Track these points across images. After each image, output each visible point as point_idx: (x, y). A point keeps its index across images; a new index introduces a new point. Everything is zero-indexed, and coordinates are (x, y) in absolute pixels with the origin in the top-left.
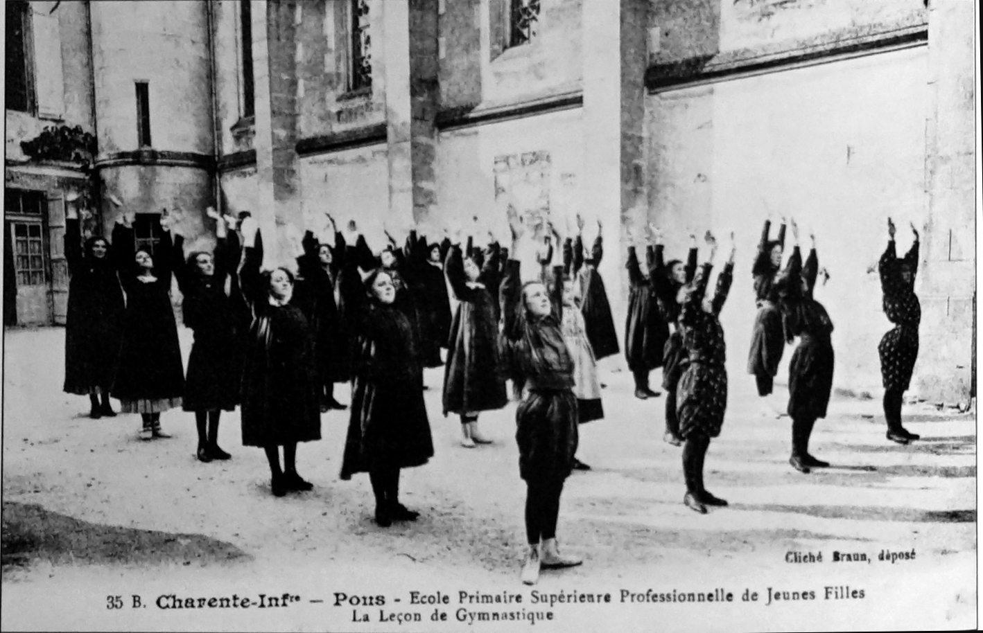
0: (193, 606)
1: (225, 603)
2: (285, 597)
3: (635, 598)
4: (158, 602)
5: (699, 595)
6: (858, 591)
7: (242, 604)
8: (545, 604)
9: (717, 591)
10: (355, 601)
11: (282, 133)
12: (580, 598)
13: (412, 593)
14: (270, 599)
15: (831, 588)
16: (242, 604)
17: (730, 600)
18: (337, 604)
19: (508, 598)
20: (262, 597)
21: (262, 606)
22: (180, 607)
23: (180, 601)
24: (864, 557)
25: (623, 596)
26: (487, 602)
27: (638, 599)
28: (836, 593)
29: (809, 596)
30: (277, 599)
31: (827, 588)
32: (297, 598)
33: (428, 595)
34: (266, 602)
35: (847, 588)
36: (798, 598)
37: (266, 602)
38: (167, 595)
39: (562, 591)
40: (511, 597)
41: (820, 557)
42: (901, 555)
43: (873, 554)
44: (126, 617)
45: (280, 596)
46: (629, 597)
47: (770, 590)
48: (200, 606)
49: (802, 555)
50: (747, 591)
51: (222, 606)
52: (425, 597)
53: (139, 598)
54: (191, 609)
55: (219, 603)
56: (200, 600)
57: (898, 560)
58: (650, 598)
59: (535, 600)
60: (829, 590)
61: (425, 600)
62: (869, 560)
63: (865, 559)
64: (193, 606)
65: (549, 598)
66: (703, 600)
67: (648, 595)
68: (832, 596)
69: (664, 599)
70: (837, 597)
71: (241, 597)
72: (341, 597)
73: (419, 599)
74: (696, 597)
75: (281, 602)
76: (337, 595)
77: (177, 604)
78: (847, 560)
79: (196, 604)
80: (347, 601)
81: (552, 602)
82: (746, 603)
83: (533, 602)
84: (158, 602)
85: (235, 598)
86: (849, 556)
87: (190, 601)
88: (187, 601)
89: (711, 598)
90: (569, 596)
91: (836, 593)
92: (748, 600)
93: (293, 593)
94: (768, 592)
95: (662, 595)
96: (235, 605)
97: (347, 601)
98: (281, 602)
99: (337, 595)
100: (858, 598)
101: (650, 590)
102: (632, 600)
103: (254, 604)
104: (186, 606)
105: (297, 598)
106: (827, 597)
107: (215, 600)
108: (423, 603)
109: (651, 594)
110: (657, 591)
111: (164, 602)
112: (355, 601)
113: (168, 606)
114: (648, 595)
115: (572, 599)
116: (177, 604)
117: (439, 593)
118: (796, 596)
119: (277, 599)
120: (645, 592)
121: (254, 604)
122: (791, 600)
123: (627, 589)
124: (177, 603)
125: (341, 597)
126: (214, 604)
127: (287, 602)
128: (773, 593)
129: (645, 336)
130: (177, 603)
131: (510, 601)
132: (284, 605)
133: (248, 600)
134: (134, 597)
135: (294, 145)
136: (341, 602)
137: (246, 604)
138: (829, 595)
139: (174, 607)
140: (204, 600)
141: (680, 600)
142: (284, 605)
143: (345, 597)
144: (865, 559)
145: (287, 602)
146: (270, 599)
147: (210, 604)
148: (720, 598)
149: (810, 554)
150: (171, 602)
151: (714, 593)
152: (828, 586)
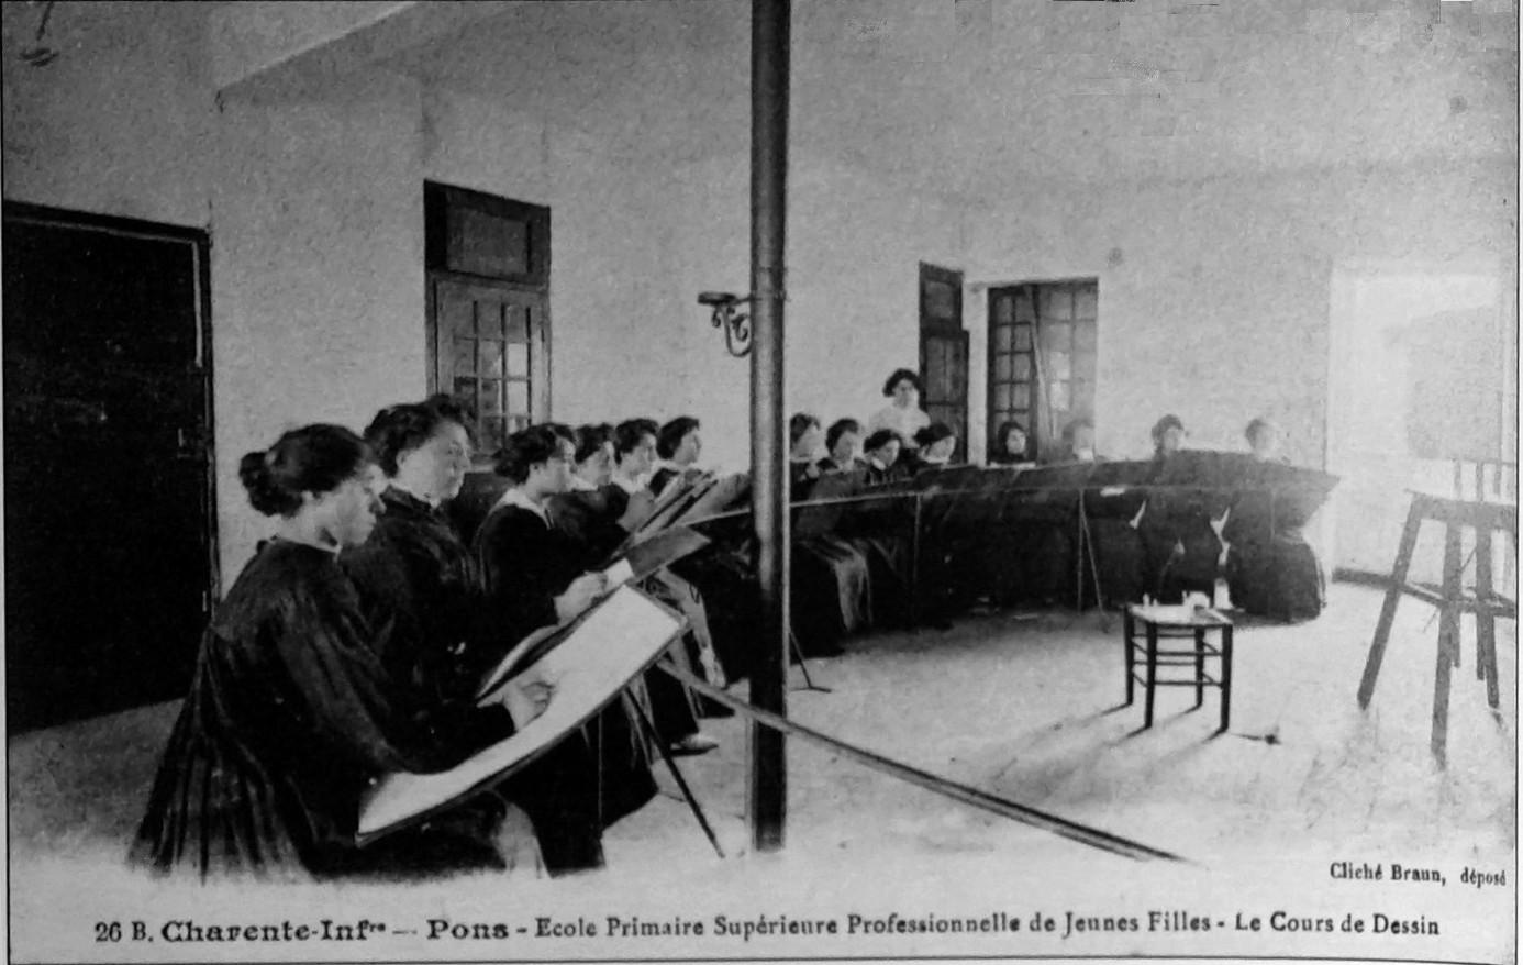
0: (220, 938)
1: (270, 934)
2: (363, 925)
3: (871, 928)
4: (165, 932)
5: (969, 922)
6: (1128, 920)
7: (298, 934)
8: (736, 936)
9: (995, 916)
10: (460, 932)
11: (777, 296)
12: (1356, 926)
13: (540, 920)
14: (340, 929)
15: (1159, 914)
16: (298, 934)
17: (1360, 931)
18: (433, 935)
19: (682, 928)
20: (327, 924)
21: (327, 936)
22: (200, 938)
23: (199, 930)
24: (1436, 875)
25: (851, 925)
26: (650, 933)
27: (876, 929)
28: (1167, 922)
29: (1129, 925)
30: (275, 930)
31: (540, 920)
32: (382, 927)
33: (564, 924)
34: (333, 932)
35: (1184, 914)
36: (1113, 928)
37: (333, 932)
38: (179, 921)
39: (762, 917)
40: (687, 926)
41: (1379, 872)
42: (1489, 879)
43: (1452, 872)
44: (126, 948)
45: (354, 925)
46: (862, 926)
47: (1069, 915)
48: (231, 938)
49: (1355, 868)
50: (1038, 915)
51: (266, 938)
52: (559, 926)
53: (144, 926)
54: (216, 942)
55: (261, 934)
56: (231, 930)
57: (1485, 885)
58: (894, 926)
59: (720, 929)
60: (1156, 917)
61: (558, 930)
62: (1444, 881)
63: (1438, 879)
64: (220, 938)
65: (743, 929)
66: (1113, 928)
67: (891, 922)
68: (1160, 926)
69: (915, 929)
70: (1167, 928)
71: (295, 925)
72: (439, 926)
73: (551, 927)
74: (1102, 923)
75: (355, 933)
76: (433, 923)
77: (194, 934)
78: (1414, 878)
79: (225, 934)
80: (448, 932)
81: (747, 933)
82: (1036, 933)
83: (716, 932)
84: (165, 932)
85: (286, 926)
86: (1416, 873)
87: (215, 930)
88: (210, 930)
89: (986, 927)
90: (772, 925)
91: (1167, 922)
92: (1039, 928)
93: (374, 920)
94: (1065, 918)
95: (912, 923)
96: (287, 937)
97: (448, 932)
98: (355, 933)
99: (433, 923)
100: (1128, 931)
101: (894, 915)
102: (866, 931)
103: (315, 933)
104: (209, 937)
105: (382, 927)
106: (1152, 928)
107: (255, 929)
108: (558, 935)
109: (896, 921)
110: (906, 915)
111: (173, 932)
112: (460, 932)
113: (179, 938)
114: (891, 922)
115: (778, 929)
116: (194, 934)
117: (581, 921)
118: (972, 926)
119: (349, 929)
120: (886, 919)
121: (315, 933)
122: (260, 924)
123: (859, 913)
124: (194, 932)
125: (439, 926)
126: (253, 935)
127: (366, 932)
128: (1074, 920)
129: (600, 804)
130: (194, 932)
131: (686, 932)
132: (361, 937)
133: (306, 928)
134: (135, 925)
135: (655, 452)
136: (438, 934)
137: (304, 934)
138: (1156, 925)
139: (189, 938)
140: (238, 929)
141: (939, 930)
142: (361, 937)
143: (446, 926)
144: (1438, 879)
145: (366, 932)
146: (340, 929)
147: (246, 935)
148: (1181, 925)
149: (1365, 866)
150: (184, 931)
151: (992, 920)
152: (1153, 910)
